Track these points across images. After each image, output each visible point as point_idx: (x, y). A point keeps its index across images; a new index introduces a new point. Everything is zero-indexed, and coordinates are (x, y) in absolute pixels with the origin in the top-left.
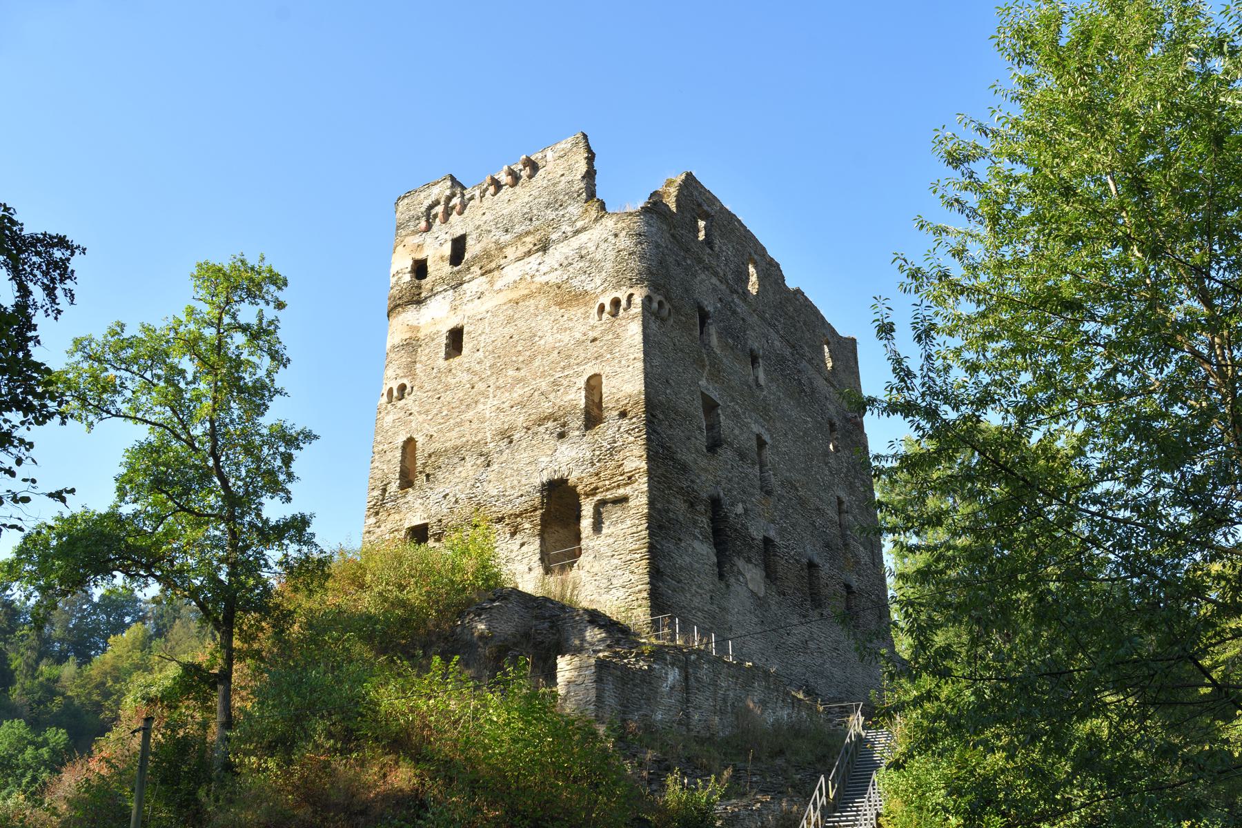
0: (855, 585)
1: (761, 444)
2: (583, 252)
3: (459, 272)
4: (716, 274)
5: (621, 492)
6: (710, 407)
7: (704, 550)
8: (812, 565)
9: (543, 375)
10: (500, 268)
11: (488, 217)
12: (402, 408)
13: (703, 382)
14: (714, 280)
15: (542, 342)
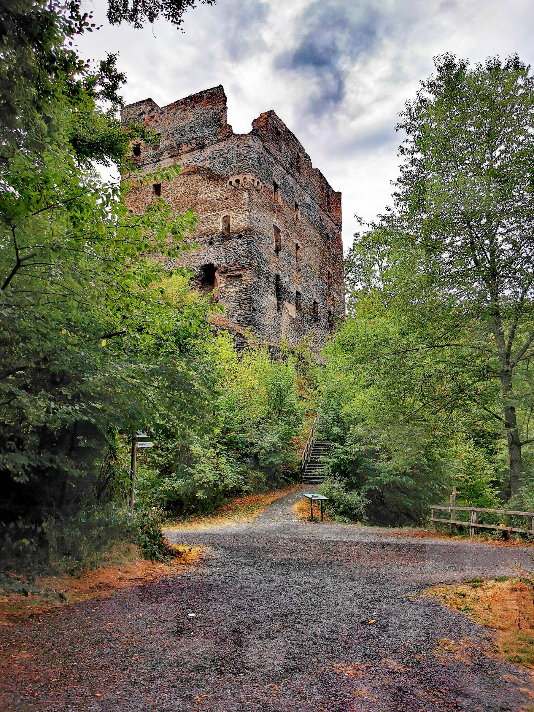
1: (298, 248)
2: (221, 153)
4: (282, 165)
5: (238, 273)
6: (277, 231)
7: (273, 299)
8: (315, 303)
10: (178, 155)
11: (171, 125)
13: (274, 220)
14: (281, 168)
15: (201, 197)
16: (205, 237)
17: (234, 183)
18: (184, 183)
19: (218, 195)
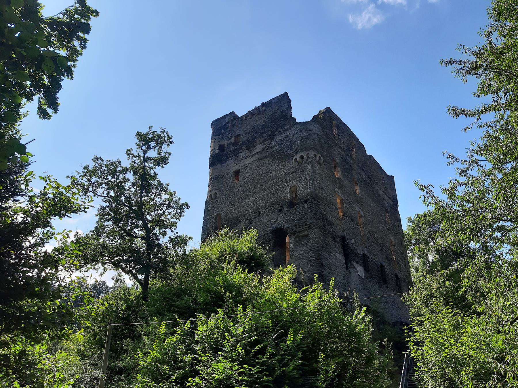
0: (399, 276)
2: (288, 139)
3: (237, 149)
4: (340, 147)
7: (341, 257)
8: (382, 266)
9: (272, 187)
11: (249, 127)
12: (215, 202)
14: (339, 150)
15: (272, 174)
16: (276, 206)
17: (298, 159)
18: (258, 167)
19: (286, 171)
